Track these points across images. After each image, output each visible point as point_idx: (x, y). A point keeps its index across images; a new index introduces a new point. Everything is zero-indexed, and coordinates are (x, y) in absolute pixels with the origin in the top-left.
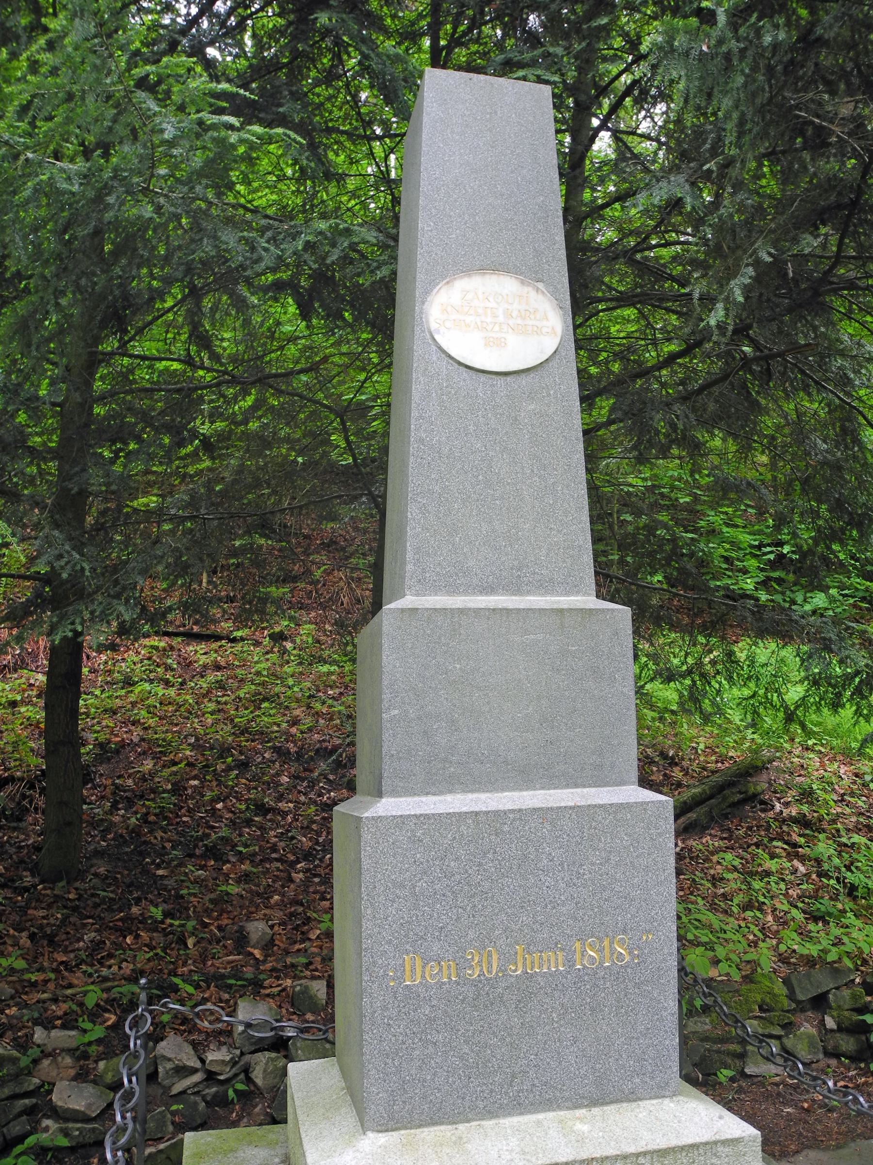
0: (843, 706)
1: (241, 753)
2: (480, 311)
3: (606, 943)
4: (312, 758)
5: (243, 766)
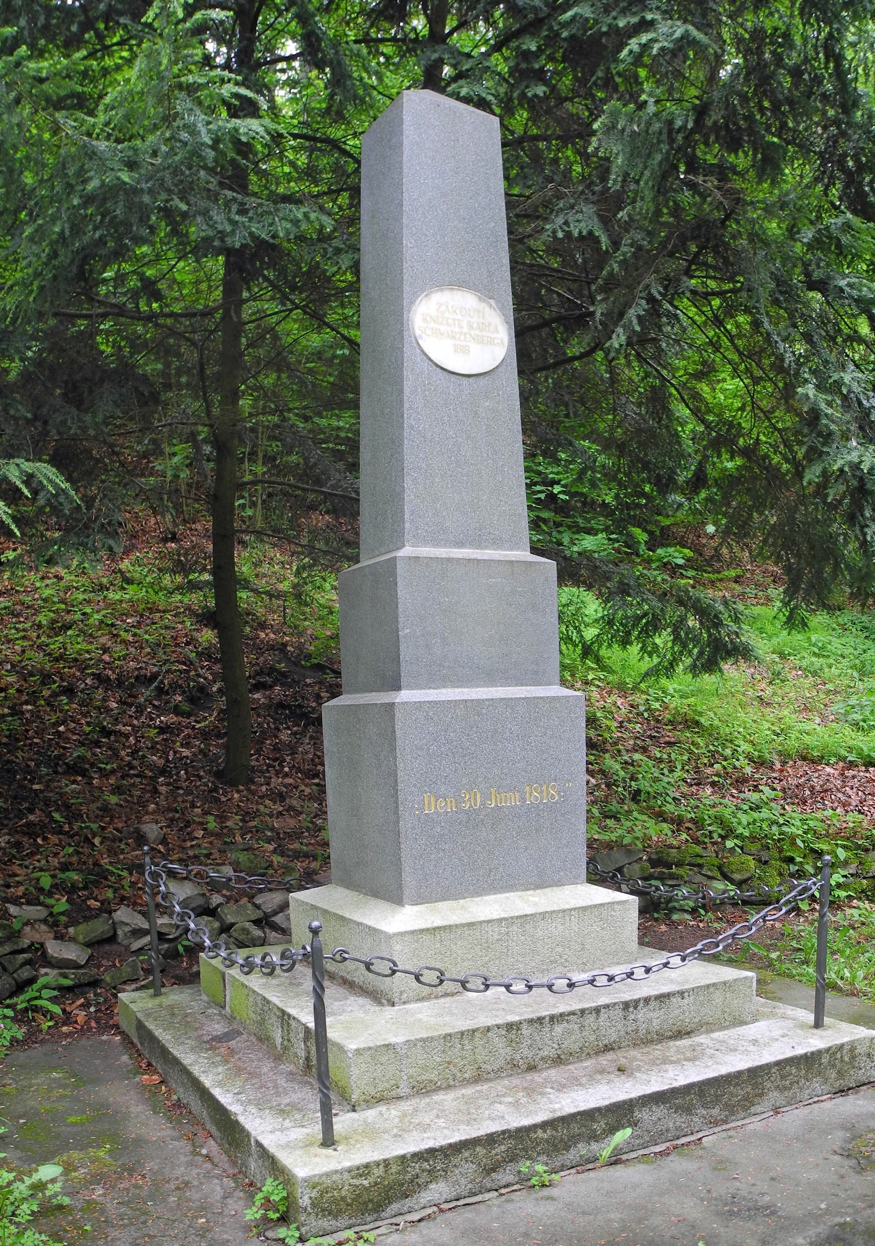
0: (631, 644)
1: (62, 680)
2: (450, 321)
3: (544, 788)
4: (132, 685)
5: (69, 691)
